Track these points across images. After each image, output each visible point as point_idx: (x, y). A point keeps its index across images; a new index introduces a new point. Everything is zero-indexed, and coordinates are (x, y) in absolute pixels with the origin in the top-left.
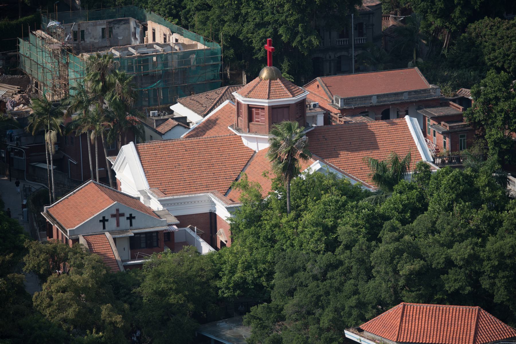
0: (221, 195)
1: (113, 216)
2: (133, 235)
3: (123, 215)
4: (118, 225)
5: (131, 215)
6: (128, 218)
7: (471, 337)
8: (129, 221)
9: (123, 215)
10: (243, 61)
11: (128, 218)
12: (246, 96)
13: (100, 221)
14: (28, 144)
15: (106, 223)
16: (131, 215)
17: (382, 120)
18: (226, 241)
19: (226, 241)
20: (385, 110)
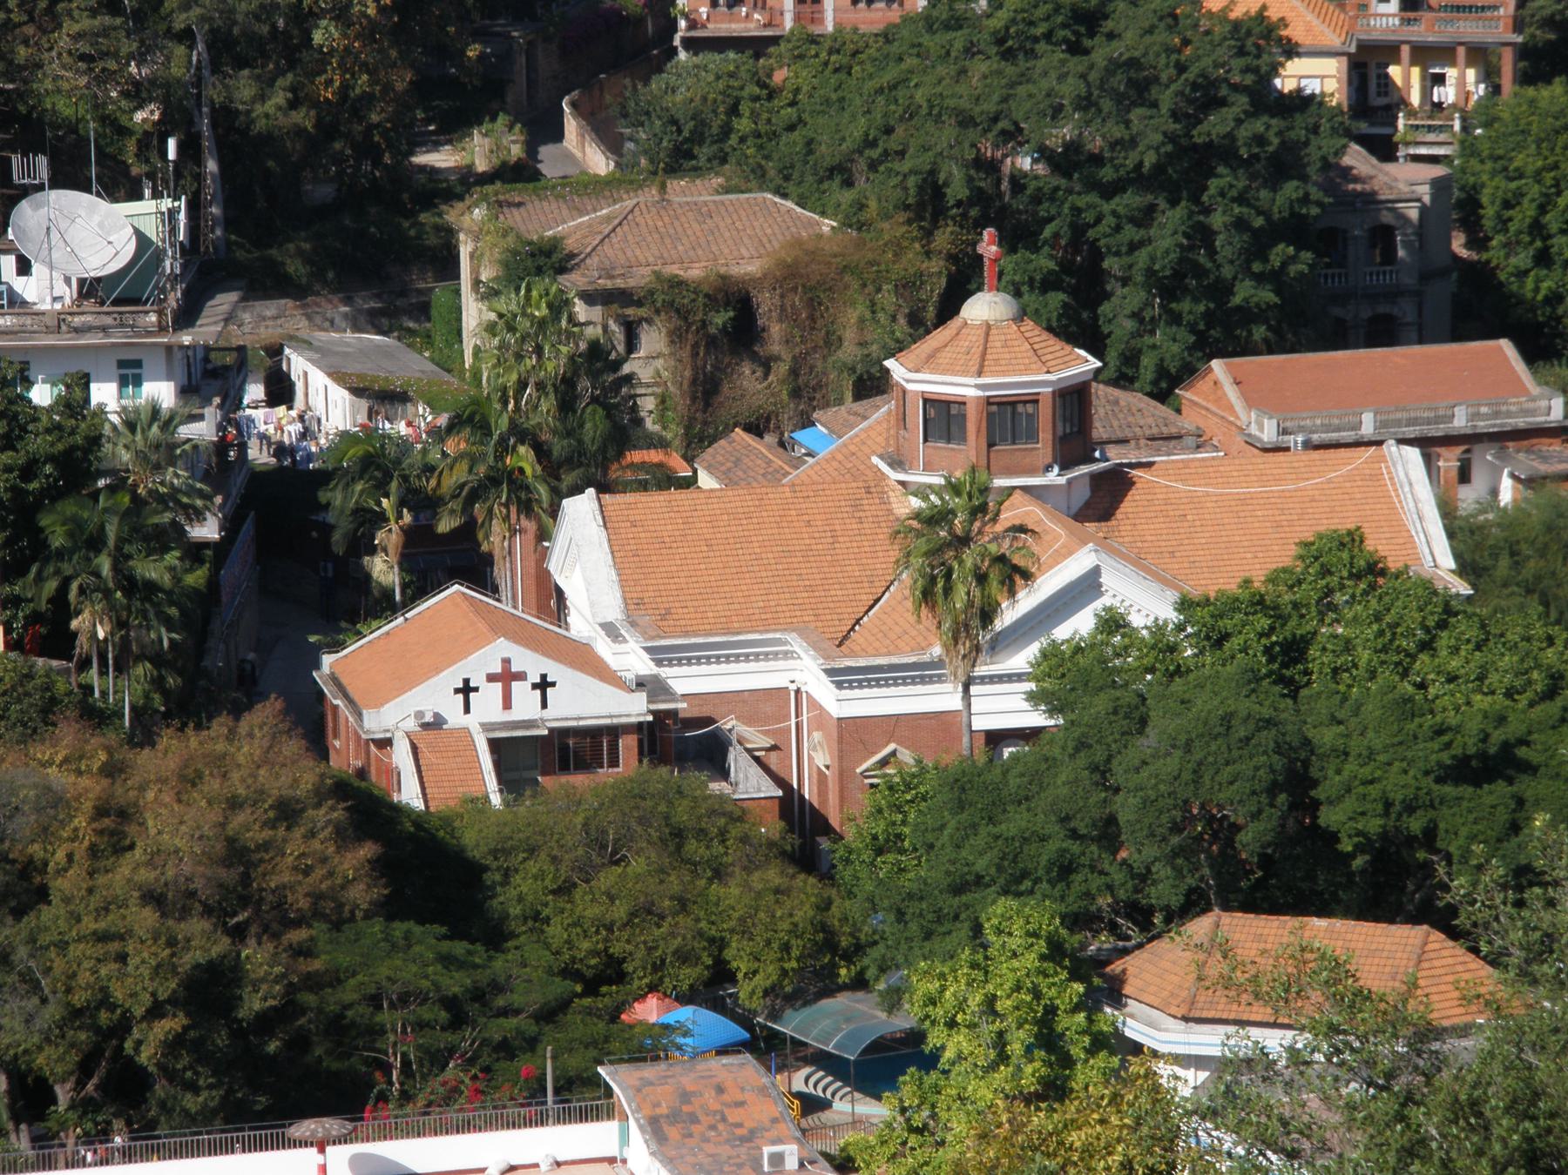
0: (827, 645)
1: (491, 678)
2: (546, 732)
3: (521, 676)
4: (507, 704)
5: (544, 677)
6: (535, 686)
7: (1427, 551)
8: (538, 692)
9: (521, 676)
10: (281, 23)
11: (535, 686)
12: (980, 374)
13: (457, 691)
14: (1412, 422)
15: (472, 695)
16: (544, 677)
17: (227, 1121)
18: (827, 767)
19: (827, 767)
20: (322, 692)
